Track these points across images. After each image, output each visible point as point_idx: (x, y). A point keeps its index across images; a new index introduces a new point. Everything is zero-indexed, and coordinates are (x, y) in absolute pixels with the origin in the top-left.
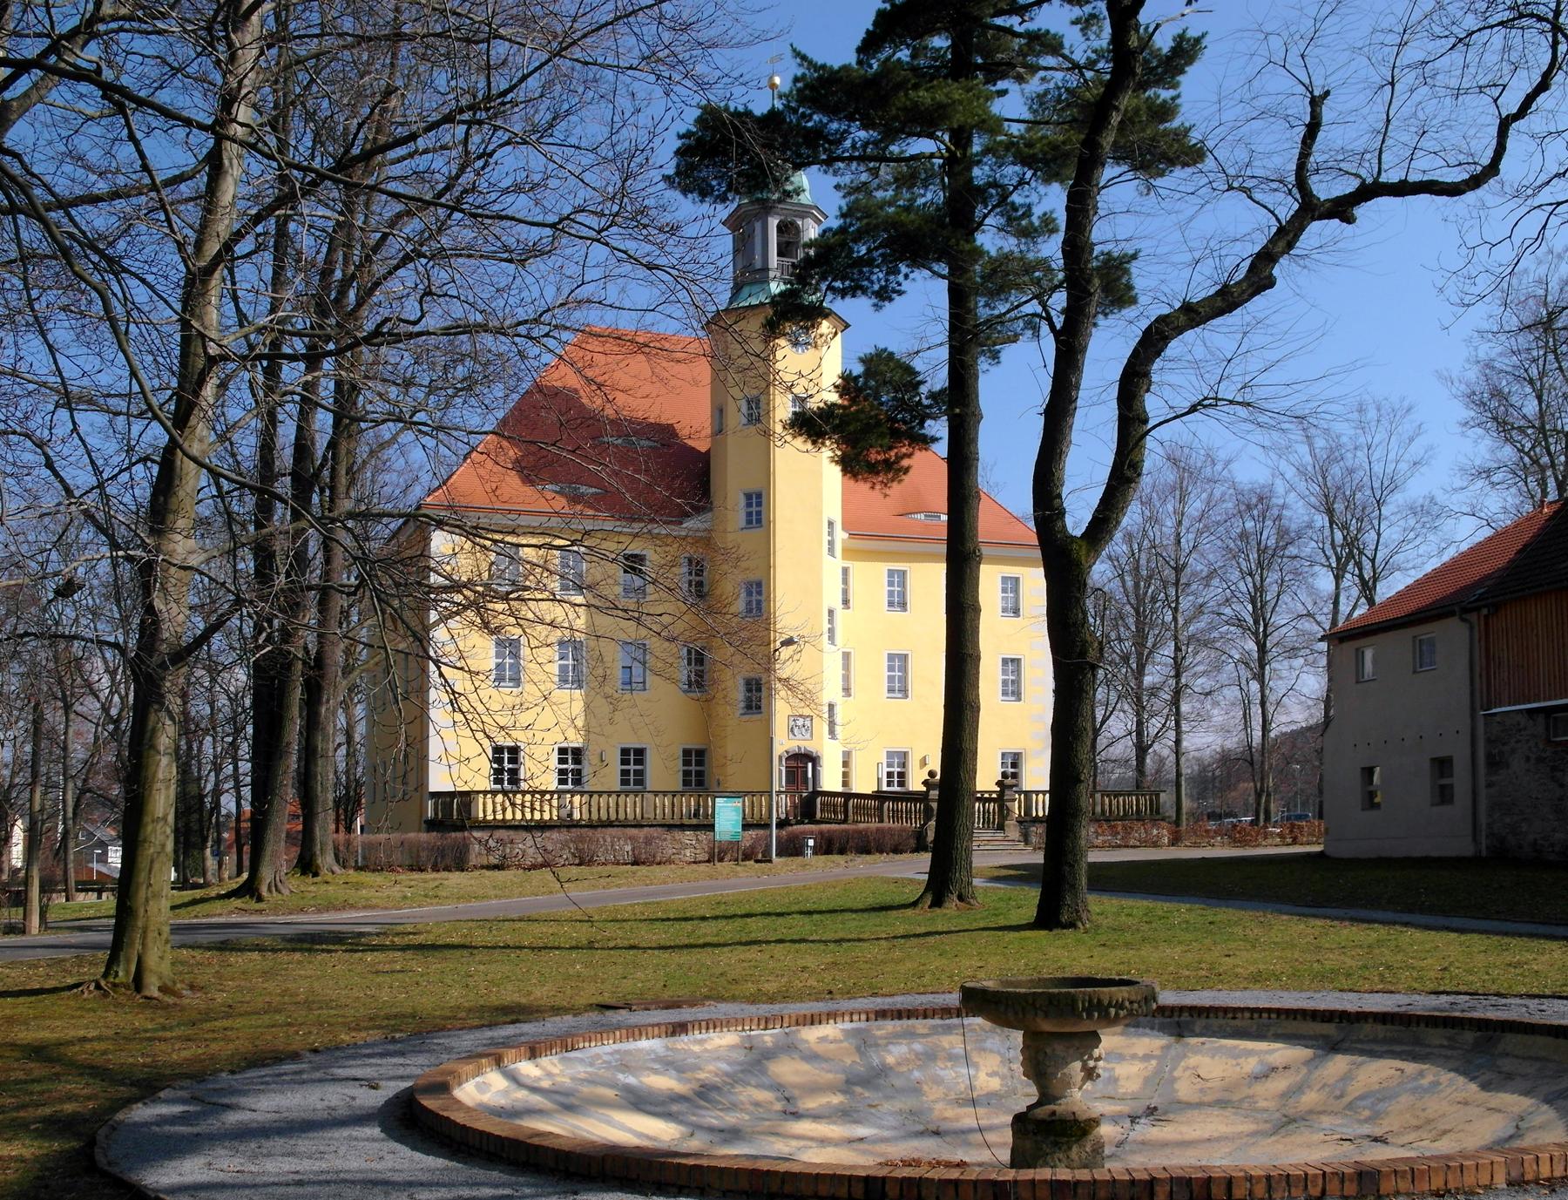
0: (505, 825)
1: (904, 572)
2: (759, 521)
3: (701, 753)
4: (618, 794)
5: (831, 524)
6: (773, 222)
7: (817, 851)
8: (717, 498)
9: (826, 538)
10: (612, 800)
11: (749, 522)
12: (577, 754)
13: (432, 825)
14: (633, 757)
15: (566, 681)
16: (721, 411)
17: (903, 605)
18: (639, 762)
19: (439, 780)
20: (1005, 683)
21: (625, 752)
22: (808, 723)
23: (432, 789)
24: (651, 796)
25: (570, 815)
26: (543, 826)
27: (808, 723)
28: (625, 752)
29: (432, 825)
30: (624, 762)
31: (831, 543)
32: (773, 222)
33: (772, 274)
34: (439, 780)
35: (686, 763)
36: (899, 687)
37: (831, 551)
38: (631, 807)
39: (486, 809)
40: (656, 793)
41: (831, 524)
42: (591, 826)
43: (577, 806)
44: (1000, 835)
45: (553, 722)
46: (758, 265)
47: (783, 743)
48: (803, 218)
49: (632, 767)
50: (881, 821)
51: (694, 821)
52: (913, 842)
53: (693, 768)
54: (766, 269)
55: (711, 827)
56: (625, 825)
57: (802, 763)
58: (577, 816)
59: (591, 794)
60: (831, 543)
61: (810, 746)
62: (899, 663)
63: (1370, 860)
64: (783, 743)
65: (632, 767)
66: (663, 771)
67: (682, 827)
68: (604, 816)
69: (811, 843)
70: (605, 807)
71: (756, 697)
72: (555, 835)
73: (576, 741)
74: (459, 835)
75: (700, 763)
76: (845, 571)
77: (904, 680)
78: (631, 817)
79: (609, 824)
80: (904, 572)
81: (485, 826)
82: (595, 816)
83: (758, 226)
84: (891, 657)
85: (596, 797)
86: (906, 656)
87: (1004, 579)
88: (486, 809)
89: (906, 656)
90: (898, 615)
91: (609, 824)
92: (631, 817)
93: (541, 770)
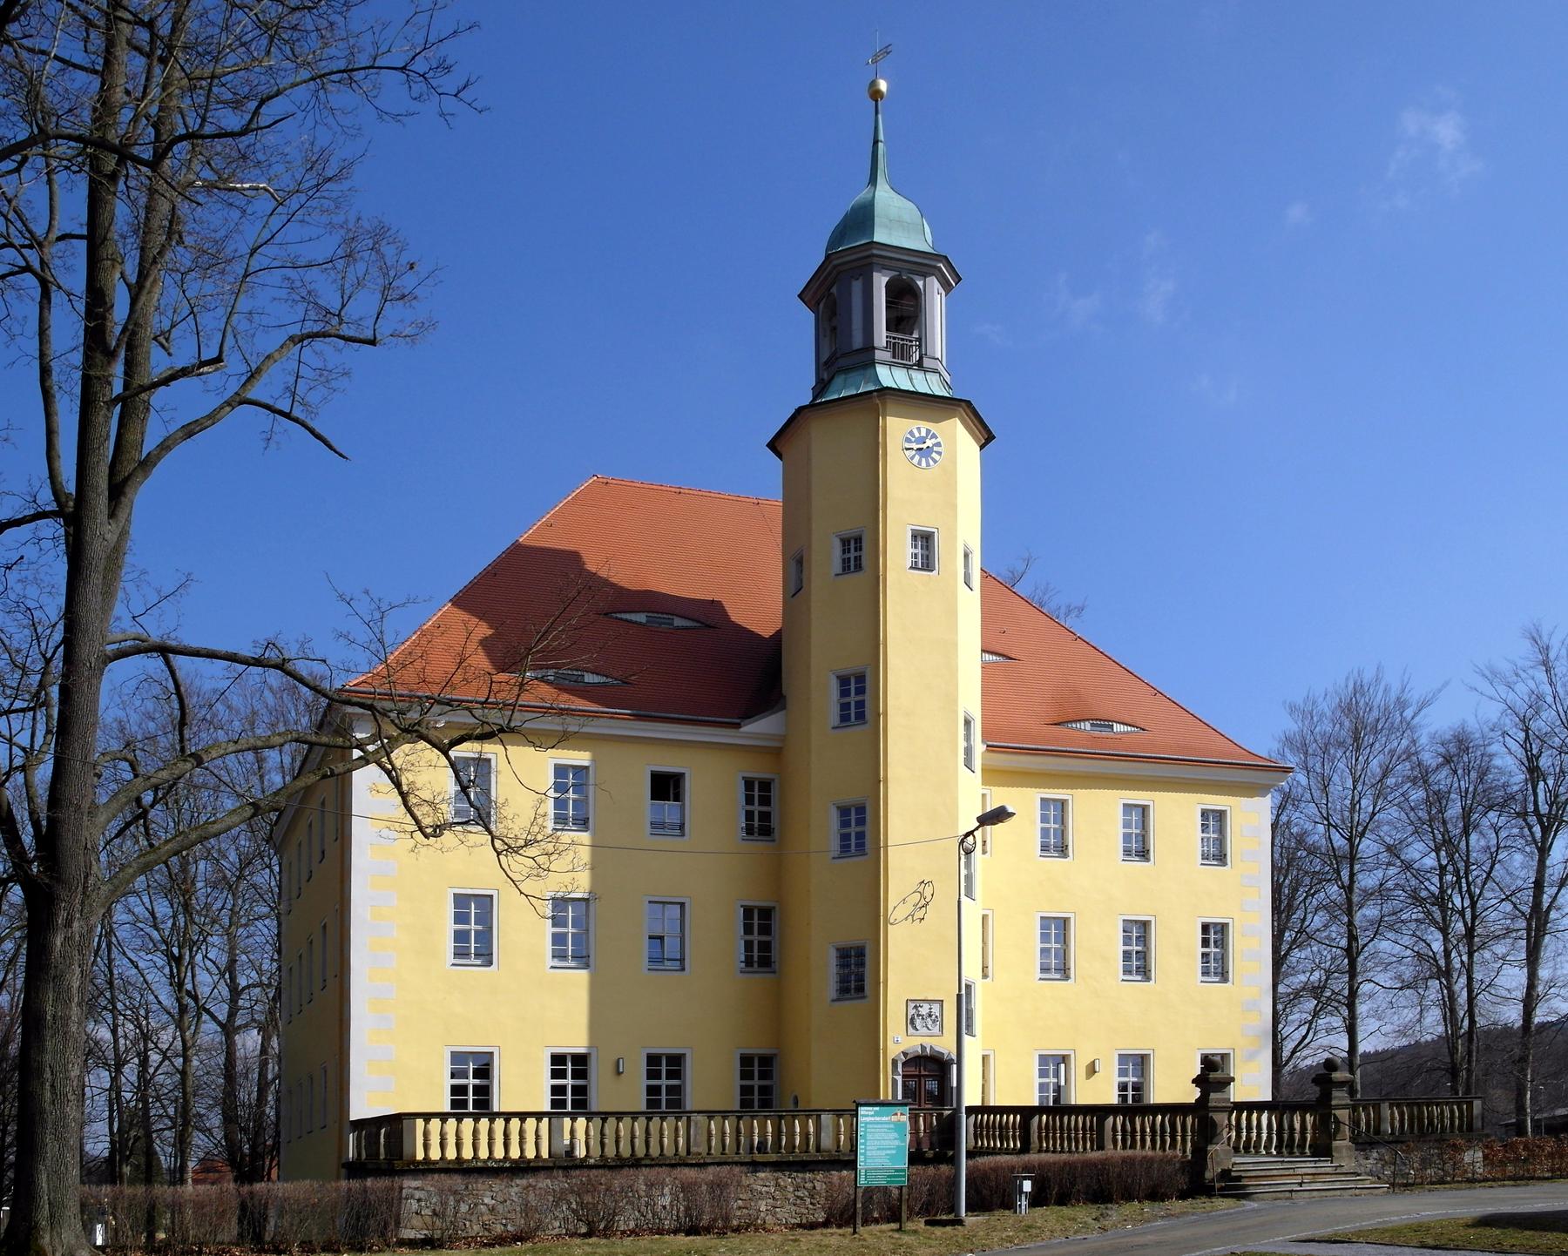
0: (460, 1168)
1: (1063, 803)
2: (861, 716)
3: (767, 1061)
4: (443, 1117)
6: (881, 281)
7: (1037, 1200)
8: (789, 685)
9: (962, 744)
10: (639, 1128)
11: (845, 718)
12: (580, 1060)
13: (355, 1170)
14: (666, 1069)
15: (466, 955)
16: (800, 562)
17: (1063, 850)
18: (675, 1074)
19: (364, 1103)
20: (1127, 956)
21: (653, 1060)
22: (936, 1009)
23: (353, 1117)
24: (701, 1118)
25: (570, 1151)
26: (521, 1168)
27: (936, 1009)
28: (653, 1060)
29: (355, 1170)
30: (653, 1074)
31: (968, 752)
32: (881, 281)
33: (879, 355)
34: (364, 1103)
35: (745, 1075)
36: (1216, 964)
37: (968, 764)
38: (668, 1135)
39: (428, 1144)
40: (711, 1115)
41: (967, 723)
42: (604, 1164)
43: (579, 1133)
44: (1325, 1165)
45: (535, 1012)
46: (858, 342)
47: (898, 1041)
48: (924, 276)
49: (664, 1082)
50: (1101, 1147)
51: (773, 1157)
52: (1182, 1181)
53: (756, 1082)
54: (869, 348)
55: (852, 1164)
56: (660, 1162)
57: (931, 1076)
58: (580, 1152)
59: (604, 1116)
60: (968, 752)
62: (1214, 935)
63: (1128, 1196)
64: (898, 1041)
65: (569, 1082)
66: (711, 1081)
67: (755, 1166)
68: (625, 1151)
69: (1027, 1186)
70: (629, 1136)
71: (857, 972)
72: (544, 1183)
73: (577, 1042)
74: (383, 1183)
75: (764, 1075)
76: (984, 796)
77: (1064, 955)
78: (640, 1152)
79: (635, 1163)
80: (1063, 803)
81: (427, 1168)
82: (610, 1152)
83: (857, 286)
84: (1046, 922)
85: (612, 1121)
86: (1065, 921)
87: (1128, 808)
88: (428, 1144)
89: (1065, 921)
90: (1056, 863)
91: (635, 1163)
92: (640, 1152)
93: (524, 1085)
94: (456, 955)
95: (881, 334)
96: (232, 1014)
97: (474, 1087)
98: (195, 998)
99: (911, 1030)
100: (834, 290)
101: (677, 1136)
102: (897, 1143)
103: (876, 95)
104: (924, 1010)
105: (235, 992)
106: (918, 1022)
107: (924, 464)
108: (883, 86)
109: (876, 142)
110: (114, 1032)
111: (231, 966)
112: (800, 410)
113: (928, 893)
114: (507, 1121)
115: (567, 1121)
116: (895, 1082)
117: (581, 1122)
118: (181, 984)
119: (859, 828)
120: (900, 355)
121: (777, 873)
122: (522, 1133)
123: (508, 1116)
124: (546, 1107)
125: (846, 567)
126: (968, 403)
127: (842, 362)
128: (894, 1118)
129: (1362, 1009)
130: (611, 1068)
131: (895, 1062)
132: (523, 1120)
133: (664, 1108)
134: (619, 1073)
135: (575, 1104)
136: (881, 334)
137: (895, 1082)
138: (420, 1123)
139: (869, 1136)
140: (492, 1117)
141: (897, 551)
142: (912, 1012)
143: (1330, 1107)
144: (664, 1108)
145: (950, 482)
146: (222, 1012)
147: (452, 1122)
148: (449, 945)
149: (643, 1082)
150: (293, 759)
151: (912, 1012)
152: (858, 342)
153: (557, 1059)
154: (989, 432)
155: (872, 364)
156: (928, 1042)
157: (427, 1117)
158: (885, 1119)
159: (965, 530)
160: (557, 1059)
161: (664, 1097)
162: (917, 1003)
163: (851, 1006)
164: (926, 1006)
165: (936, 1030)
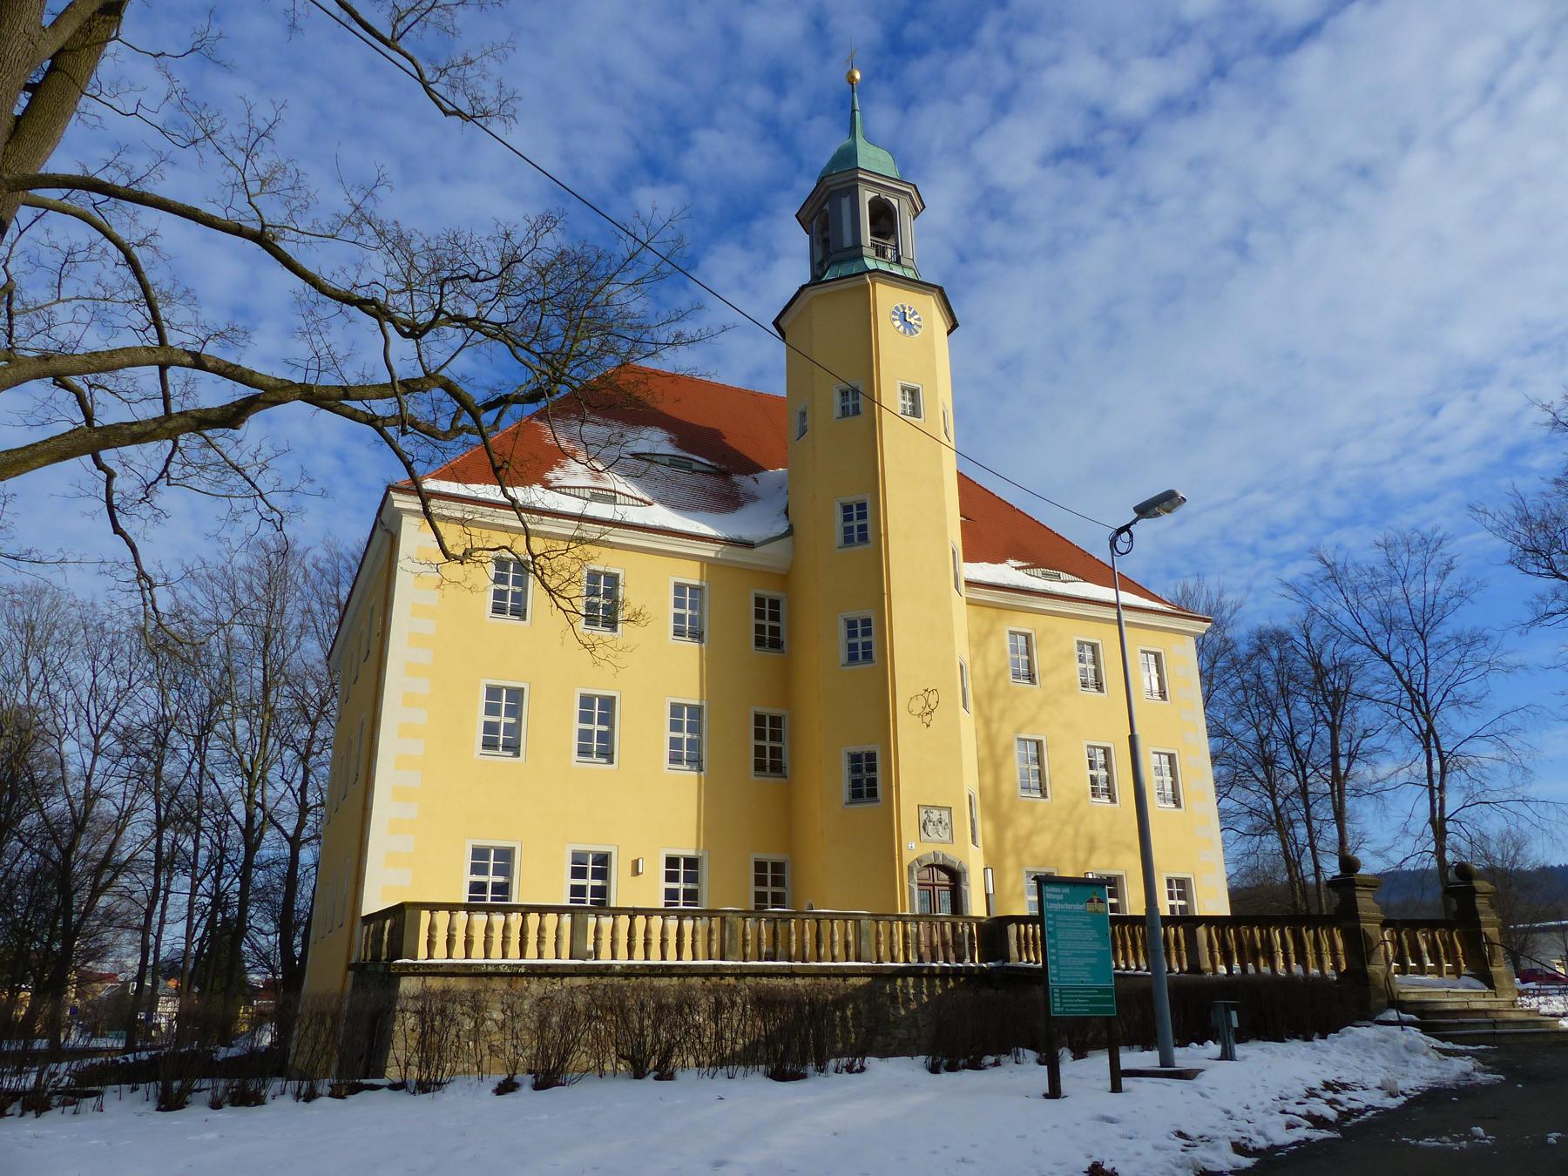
12: (691, 863)
33: (866, 251)
47: (913, 847)
54: (858, 246)
65: (680, 886)
71: (868, 779)
83: (846, 203)
95: (867, 237)
96: (299, 829)
97: (492, 887)
98: (262, 807)
100: (826, 207)
101: (710, 940)
102: (1097, 946)
103: (851, 80)
104: (935, 816)
105: (304, 809)
106: (930, 827)
108: (858, 76)
109: (853, 111)
110: (196, 842)
111: (303, 789)
112: (803, 288)
113: (932, 699)
115: (592, 921)
116: (911, 890)
118: (250, 796)
119: (865, 642)
121: (785, 683)
122: (541, 929)
123: (526, 910)
125: (845, 412)
126: (941, 290)
127: (835, 257)
131: (910, 869)
134: (636, 872)
136: (867, 237)
137: (911, 890)
138: (425, 916)
139: (1060, 935)
140: (507, 910)
141: (890, 397)
142: (924, 816)
143: (1357, 918)
145: (930, 346)
146: (290, 826)
148: (479, 735)
151: (924, 816)
152: (848, 241)
153: (672, 862)
155: (861, 257)
156: (940, 848)
157: (434, 907)
158: (1078, 907)
159: (941, 396)
160: (672, 862)
162: (929, 808)
163: (864, 808)
164: (936, 812)
165: (946, 837)
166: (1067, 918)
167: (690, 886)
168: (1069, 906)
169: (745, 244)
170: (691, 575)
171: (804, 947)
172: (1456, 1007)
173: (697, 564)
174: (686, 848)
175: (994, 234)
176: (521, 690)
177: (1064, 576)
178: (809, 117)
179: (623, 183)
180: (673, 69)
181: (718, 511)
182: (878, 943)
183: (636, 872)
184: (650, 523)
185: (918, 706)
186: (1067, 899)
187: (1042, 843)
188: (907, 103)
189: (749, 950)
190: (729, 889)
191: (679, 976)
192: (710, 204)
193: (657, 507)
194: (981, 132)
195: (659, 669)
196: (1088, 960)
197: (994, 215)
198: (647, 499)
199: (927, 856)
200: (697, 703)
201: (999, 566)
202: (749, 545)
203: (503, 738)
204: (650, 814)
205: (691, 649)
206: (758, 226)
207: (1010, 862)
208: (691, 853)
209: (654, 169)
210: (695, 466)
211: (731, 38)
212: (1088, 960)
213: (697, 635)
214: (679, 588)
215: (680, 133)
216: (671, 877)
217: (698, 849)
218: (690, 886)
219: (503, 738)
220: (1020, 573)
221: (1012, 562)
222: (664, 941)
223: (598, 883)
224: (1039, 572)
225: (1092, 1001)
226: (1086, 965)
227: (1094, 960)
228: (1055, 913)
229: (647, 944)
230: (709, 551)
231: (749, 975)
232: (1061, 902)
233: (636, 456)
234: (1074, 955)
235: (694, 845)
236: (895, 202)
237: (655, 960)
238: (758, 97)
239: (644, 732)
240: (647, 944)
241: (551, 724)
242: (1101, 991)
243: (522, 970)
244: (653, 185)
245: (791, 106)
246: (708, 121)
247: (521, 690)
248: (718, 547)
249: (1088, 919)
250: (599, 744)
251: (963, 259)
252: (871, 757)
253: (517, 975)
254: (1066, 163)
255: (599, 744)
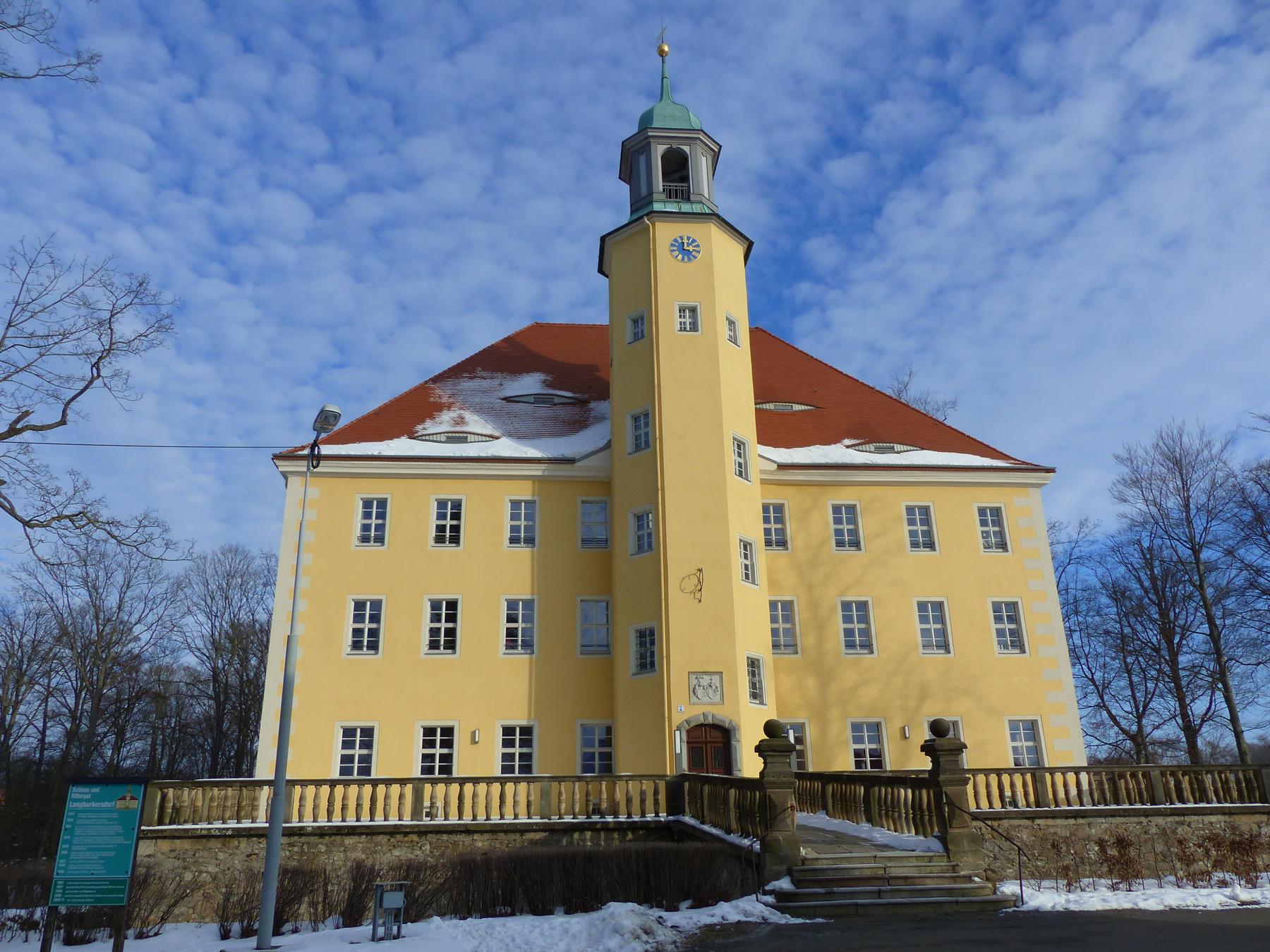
4: (333, 783)
5: (740, 445)
12: (526, 731)
18: (367, 745)
33: (655, 196)
49: (438, 751)
54: (650, 193)
61: (722, 713)
62: (1008, 613)
64: (684, 709)
65: (517, 750)
83: (642, 159)
93: (479, 756)
94: (508, 647)
95: (659, 183)
99: (694, 699)
102: (120, 840)
103: (662, 54)
106: (699, 691)
107: (680, 257)
108: (666, 48)
114: (461, 785)
117: (523, 786)
120: (671, 194)
124: (417, 773)
128: (121, 804)
129: (1233, 682)
130: (898, 735)
132: (461, 785)
133: (437, 775)
134: (474, 742)
135: (442, 770)
139: (78, 831)
140: (448, 782)
144: (437, 775)
147: (339, 789)
149: (499, 750)
150: (1139, 580)
153: (508, 731)
154: (747, 239)
156: (708, 709)
158: (106, 805)
160: (508, 731)
161: (437, 764)
162: (699, 674)
164: (707, 678)
166: (90, 815)
167: (525, 750)
168: (95, 805)
169: (921, 187)
170: (524, 492)
171: (573, 805)
172: (868, 873)
173: (529, 484)
174: (519, 720)
175: (1150, 130)
176: (380, 601)
177: (898, 447)
178: (970, 70)
179: (816, 161)
180: (852, 60)
181: (578, 431)
182: (560, 802)
183: (474, 742)
184: (483, 454)
185: (690, 584)
186: (95, 798)
187: (869, 694)
188: (1059, 33)
189: (563, 806)
190: (557, 754)
191: (367, 834)
192: (891, 161)
193: (505, 441)
194: (1129, 45)
195: (492, 573)
196: (104, 854)
197: (1148, 114)
198: (496, 434)
199: (696, 717)
200: (528, 597)
201: (833, 447)
202: (571, 461)
203: (366, 640)
204: (488, 693)
205: (523, 553)
206: (931, 169)
207: (834, 713)
208: (524, 723)
209: (842, 144)
210: (556, 400)
211: (898, 21)
212: (104, 854)
213: (530, 541)
214: (515, 504)
215: (859, 111)
216: (506, 743)
217: (529, 719)
218: (525, 750)
219: (366, 640)
220: (850, 450)
221: (847, 442)
222: (359, 806)
223: (445, 751)
224: (871, 447)
225: (99, 891)
226: (101, 858)
227: (112, 854)
228: (77, 811)
229: (344, 808)
230: (536, 470)
231: (431, 832)
232: (87, 801)
233: (508, 399)
234: (89, 850)
235: (525, 715)
236: (686, 149)
237: (351, 821)
238: (926, 66)
239: (482, 626)
240: (344, 808)
241: (407, 626)
242: (112, 882)
243: (230, 833)
244: (841, 156)
245: (955, 64)
246: (884, 95)
247: (380, 601)
248: (543, 466)
249: (115, 815)
250: (444, 639)
251: (1121, 159)
252: (652, 633)
253: (225, 836)
254: (1221, 50)
255: (444, 639)
